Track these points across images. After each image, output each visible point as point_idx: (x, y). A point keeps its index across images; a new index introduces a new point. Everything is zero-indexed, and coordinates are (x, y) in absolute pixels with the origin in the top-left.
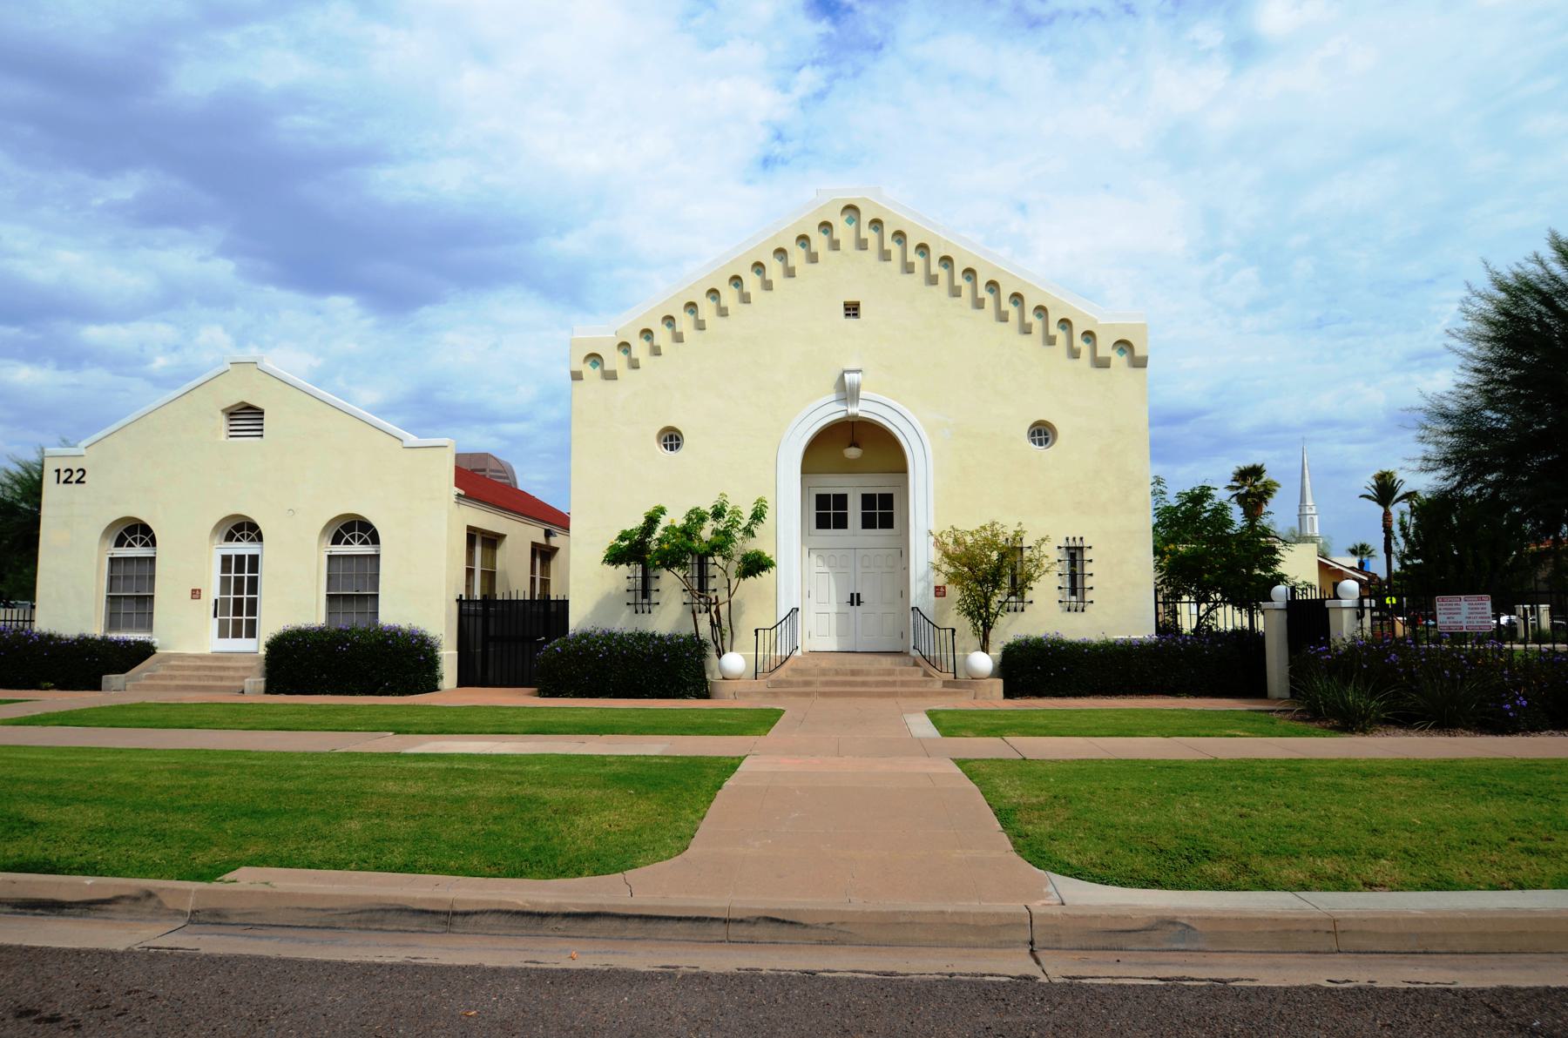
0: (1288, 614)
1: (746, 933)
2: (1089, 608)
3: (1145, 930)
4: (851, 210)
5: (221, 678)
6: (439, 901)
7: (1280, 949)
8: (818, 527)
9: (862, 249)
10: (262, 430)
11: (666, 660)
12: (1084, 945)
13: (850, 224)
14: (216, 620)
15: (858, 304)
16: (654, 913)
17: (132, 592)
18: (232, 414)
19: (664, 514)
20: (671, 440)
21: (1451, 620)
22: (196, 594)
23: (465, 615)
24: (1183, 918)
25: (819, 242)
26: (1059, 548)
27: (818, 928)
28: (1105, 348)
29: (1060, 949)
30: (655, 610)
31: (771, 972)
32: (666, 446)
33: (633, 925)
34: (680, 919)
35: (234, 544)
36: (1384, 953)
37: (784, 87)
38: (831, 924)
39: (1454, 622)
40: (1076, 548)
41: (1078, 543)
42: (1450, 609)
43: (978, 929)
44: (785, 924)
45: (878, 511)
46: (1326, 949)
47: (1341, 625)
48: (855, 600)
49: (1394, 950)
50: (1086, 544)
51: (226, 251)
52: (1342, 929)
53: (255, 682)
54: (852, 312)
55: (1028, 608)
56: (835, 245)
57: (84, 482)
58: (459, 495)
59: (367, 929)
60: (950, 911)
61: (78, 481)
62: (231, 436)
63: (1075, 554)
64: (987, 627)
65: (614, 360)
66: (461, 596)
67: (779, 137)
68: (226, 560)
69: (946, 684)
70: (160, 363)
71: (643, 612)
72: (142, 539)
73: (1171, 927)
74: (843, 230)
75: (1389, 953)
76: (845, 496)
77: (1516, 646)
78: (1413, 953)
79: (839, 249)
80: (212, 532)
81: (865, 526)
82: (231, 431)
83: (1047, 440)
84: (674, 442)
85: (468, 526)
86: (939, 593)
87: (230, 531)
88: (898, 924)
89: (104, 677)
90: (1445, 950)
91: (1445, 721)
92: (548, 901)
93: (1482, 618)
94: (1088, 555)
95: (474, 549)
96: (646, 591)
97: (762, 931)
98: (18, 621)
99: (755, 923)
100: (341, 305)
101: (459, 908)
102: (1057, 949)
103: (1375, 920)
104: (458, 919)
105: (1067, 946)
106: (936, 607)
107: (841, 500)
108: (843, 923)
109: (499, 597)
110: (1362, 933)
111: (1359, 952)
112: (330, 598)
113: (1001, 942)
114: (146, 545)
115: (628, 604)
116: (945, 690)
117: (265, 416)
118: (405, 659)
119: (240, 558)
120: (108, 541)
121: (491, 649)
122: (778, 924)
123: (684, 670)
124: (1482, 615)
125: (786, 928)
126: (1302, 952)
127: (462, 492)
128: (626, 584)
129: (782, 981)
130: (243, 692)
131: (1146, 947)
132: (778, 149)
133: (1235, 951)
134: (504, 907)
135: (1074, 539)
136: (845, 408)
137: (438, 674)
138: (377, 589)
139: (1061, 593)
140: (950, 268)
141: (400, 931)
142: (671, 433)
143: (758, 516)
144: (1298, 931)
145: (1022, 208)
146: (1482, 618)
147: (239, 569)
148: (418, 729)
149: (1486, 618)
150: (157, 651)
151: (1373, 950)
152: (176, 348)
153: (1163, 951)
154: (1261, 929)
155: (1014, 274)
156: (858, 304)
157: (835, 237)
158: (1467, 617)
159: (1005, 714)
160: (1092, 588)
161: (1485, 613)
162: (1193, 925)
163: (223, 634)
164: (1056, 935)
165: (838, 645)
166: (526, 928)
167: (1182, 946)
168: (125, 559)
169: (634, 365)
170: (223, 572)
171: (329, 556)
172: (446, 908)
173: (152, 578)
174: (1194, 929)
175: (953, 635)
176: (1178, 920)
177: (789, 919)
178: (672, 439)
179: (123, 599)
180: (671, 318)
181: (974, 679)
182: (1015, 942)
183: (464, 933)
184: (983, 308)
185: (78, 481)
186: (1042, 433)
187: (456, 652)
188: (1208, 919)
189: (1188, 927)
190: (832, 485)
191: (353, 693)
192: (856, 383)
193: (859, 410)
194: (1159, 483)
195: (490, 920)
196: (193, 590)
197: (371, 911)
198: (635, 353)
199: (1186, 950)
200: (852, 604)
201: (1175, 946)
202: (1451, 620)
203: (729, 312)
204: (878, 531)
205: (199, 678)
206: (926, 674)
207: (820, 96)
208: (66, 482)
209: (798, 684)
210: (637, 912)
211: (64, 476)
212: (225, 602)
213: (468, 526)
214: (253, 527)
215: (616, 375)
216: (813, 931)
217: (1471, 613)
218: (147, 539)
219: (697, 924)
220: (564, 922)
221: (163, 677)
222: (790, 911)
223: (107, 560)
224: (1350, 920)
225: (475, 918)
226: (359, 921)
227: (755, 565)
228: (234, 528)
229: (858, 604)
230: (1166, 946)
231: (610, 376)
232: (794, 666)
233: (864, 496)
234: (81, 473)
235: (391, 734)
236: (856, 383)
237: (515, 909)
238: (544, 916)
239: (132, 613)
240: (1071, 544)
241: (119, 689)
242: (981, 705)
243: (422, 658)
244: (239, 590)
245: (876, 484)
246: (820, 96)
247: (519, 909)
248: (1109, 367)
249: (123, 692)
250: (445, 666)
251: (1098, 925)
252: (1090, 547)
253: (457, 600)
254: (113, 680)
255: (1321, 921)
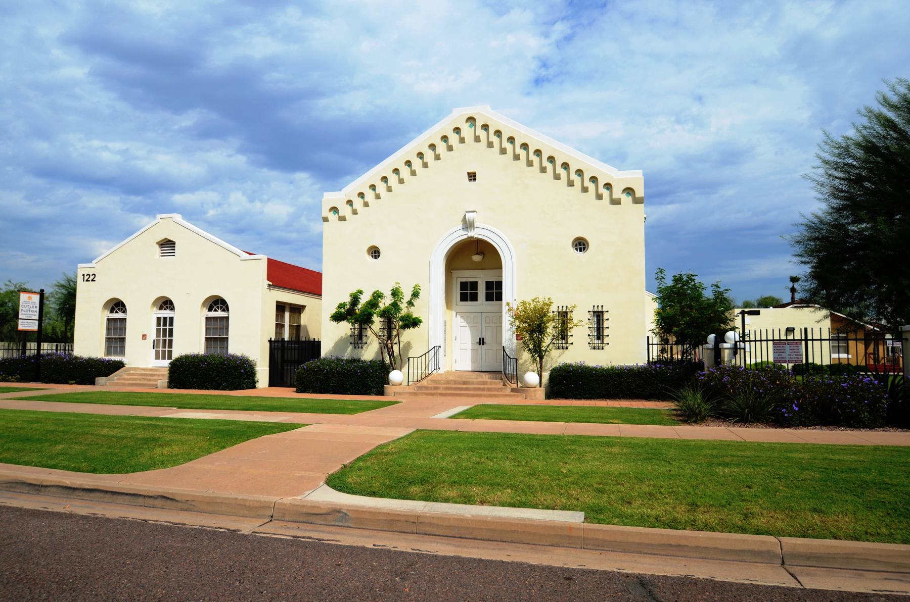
0: (715, 352)
1: (152, 503)
2: (606, 347)
3: (325, 514)
4: (471, 120)
5: (150, 380)
6: (37, 480)
7: (387, 529)
8: (461, 301)
9: (477, 142)
10: (174, 252)
11: (359, 374)
12: (295, 519)
13: (471, 128)
14: (154, 350)
15: (475, 173)
16: (117, 491)
17: (117, 336)
18: (162, 244)
19: (362, 294)
20: (375, 253)
21: (780, 357)
22: (144, 337)
23: (742, 348)
24: (344, 509)
25: (454, 139)
26: (589, 312)
27: (182, 502)
28: (617, 193)
29: (284, 521)
30: (365, 347)
31: (874, 592)
32: (576, 249)
33: (108, 496)
34: (127, 494)
35: (163, 311)
36: (439, 536)
37: (546, 35)
38: (188, 501)
39: (783, 358)
40: (598, 312)
41: (600, 309)
42: (780, 350)
43: (250, 508)
44: (169, 500)
45: (494, 291)
46: (410, 531)
47: (724, 358)
48: (481, 342)
49: (444, 534)
50: (605, 309)
51: (241, 151)
52: (420, 521)
53: (163, 382)
54: (473, 178)
55: (570, 347)
56: (462, 140)
57: (95, 281)
58: (269, 285)
59: (9, 491)
60: (240, 498)
61: (92, 280)
62: (161, 256)
63: (599, 316)
64: (541, 358)
65: (345, 210)
66: (271, 338)
67: (545, 65)
68: (159, 319)
69: (513, 390)
70: (211, 213)
71: (359, 348)
72: (170, 307)
73: (337, 514)
74: (467, 131)
75: (441, 536)
76: (476, 283)
77: (892, 374)
78: (454, 537)
79: (465, 143)
80: (103, 308)
81: (487, 300)
82: (162, 253)
83: (584, 248)
84: (377, 254)
85: (277, 302)
86: (519, 338)
87: (161, 305)
88: (216, 503)
89: (96, 378)
90: (471, 537)
91: (745, 418)
92: (78, 482)
93: (797, 355)
94: (606, 316)
95: (284, 313)
96: (360, 336)
97: (159, 502)
98: (60, 350)
99: (156, 498)
100: (302, 176)
101: (44, 484)
102: (282, 520)
103: (438, 518)
104: (43, 489)
105: (287, 520)
106: (517, 346)
107: (474, 285)
108: (193, 501)
109: (304, 340)
110: (430, 524)
111: (426, 534)
112: (207, 339)
113: (258, 515)
114: (224, 310)
115: (351, 343)
116: (512, 393)
117: (176, 245)
118: (233, 371)
119: (165, 319)
120: (205, 308)
121: (285, 368)
122: (165, 499)
123: (370, 379)
124: (797, 354)
125: (169, 502)
126: (398, 532)
127: (271, 283)
128: (349, 333)
129: (134, 523)
130: (157, 387)
131: (323, 523)
132: (543, 72)
133: (365, 529)
134: (61, 484)
135: (598, 306)
136: (467, 233)
137: (256, 380)
138: (228, 335)
139: (590, 338)
140: (527, 150)
141: (20, 492)
142: (580, 241)
143: (415, 295)
144: (398, 520)
145: (700, 99)
146: (797, 355)
147: (165, 324)
148: (190, 406)
149: (799, 355)
150: (126, 366)
151: (434, 533)
152: (220, 205)
153: (331, 525)
154: (380, 518)
155: (564, 151)
156: (475, 173)
157: (462, 136)
158: (788, 355)
159: (169, 396)
160: (608, 336)
161: (799, 352)
162: (348, 514)
163: (157, 358)
164: (284, 514)
165: (472, 367)
166: (67, 494)
167: (340, 524)
168: (114, 319)
169: (355, 212)
170: (172, 329)
171: (206, 317)
172: (38, 483)
173: (227, 328)
174: (348, 516)
175: (516, 362)
176: (342, 510)
177: (171, 497)
178: (375, 252)
179: (113, 339)
180: (374, 186)
181: (527, 387)
182: (264, 515)
183: (44, 495)
184: (546, 172)
185: (92, 280)
186: (581, 245)
187: (268, 368)
188: (356, 511)
189: (346, 514)
190: (469, 276)
191: (208, 389)
192: (472, 218)
193: (474, 234)
194: (661, 272)
195: (54, 490)
196: (143, 335)
197: (12, 483)
198: (355, 206)
199: (342, 526)
200: (480, 344)
201: (337, 524)
202: (780, 357)
203: (405, 181)
204: (469, 303)
205: (140, 380)
206: (504, 385)
207: (568, 39)
208: (87, 281)
209: (431, 389)
210: (111, 490)
211: (86, 278)
212: (158, 341)
213: (277, 302)
214: (223, 302)
215: (345, 218)
216: (180, 504)
217: (791, 352)
218: (224, 307)
219: (133, 497)
220: (82, 493)
221: (124, 379)
222: (172, 494)
223: (106, 320)
224: (426, 517)
225: (49, 488)
226: (7, 487)
227: (411, 323)
228: (163, 303)
229: (483, 344)
230: (333, 523)
231: (342, 219)
232: (435, 379)
233: (487, 283)
234: (94, 276)
235: (175, 408)
236: (472, 218)
237: (64, 485)
238: (75, 489)
239: (224, 347)
240: (596, 309)
241: (103, 384)
242: (529, 402)
243: (242, 371)
244: (164, 335)
245: (490, 276)
246: (568, 39)
247: (67, 485)
248: (620, 204)
249: (105, 386)
250: (259, 376)
251: (304, 510)
252: (607, 311)
253: (269, 341)
254: (100, 380)
255: (411, 516)
